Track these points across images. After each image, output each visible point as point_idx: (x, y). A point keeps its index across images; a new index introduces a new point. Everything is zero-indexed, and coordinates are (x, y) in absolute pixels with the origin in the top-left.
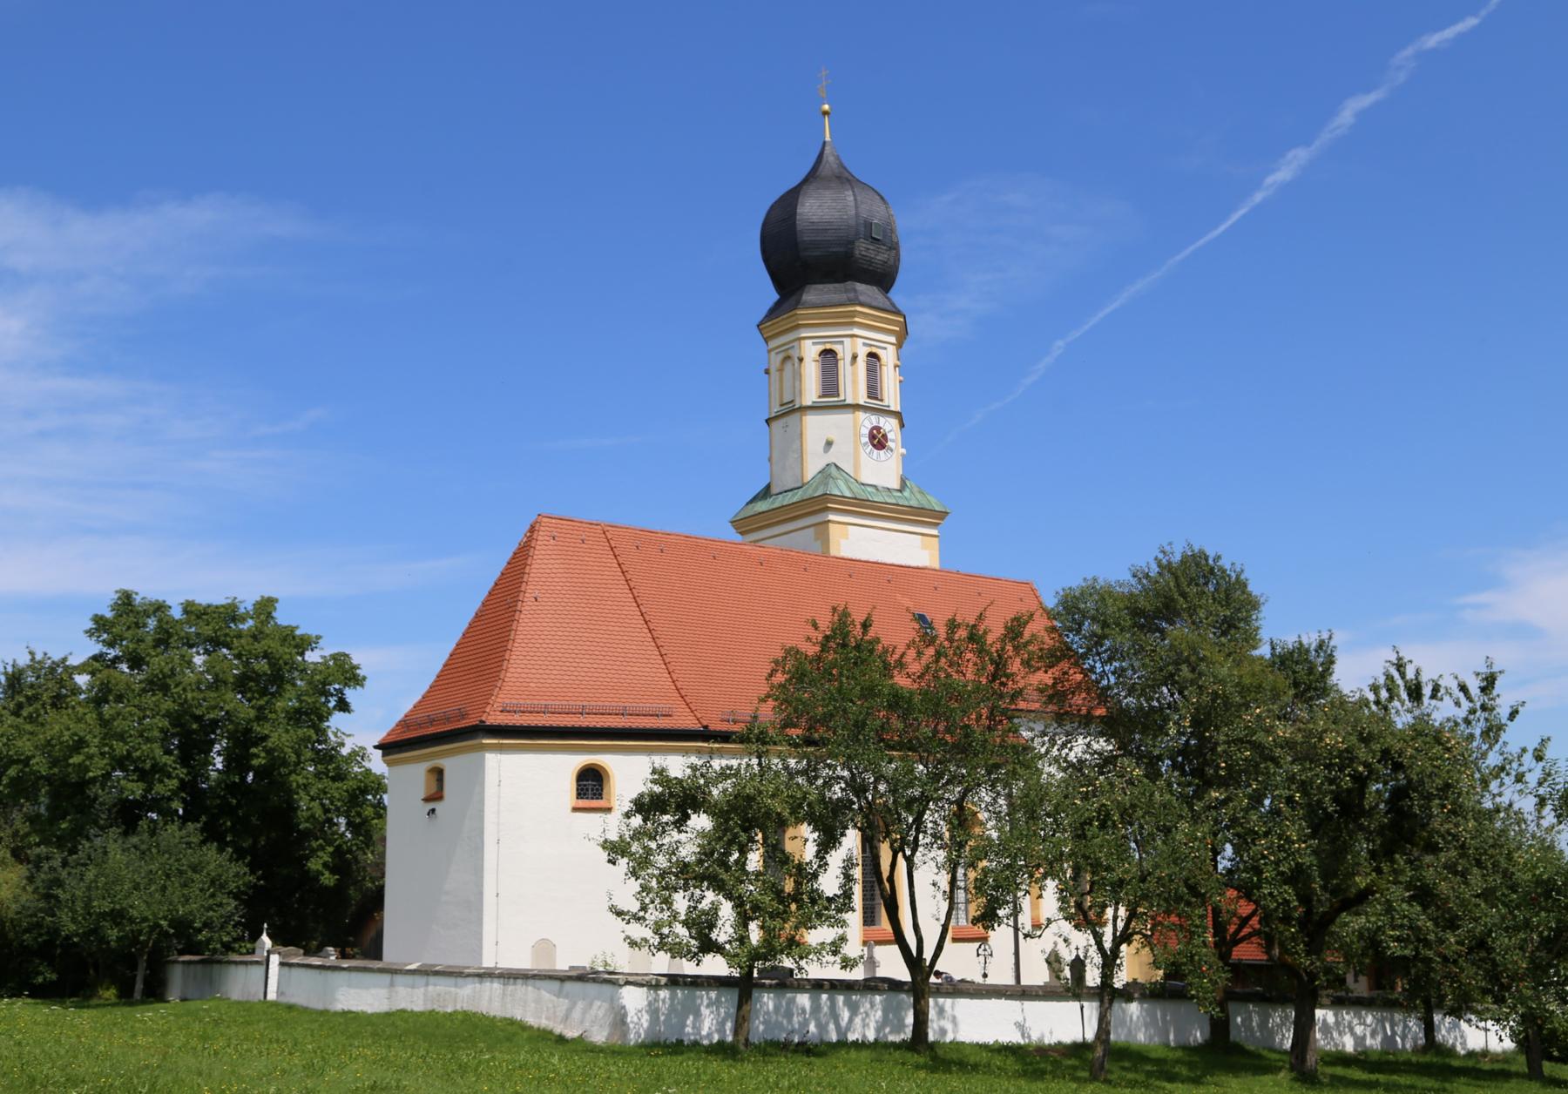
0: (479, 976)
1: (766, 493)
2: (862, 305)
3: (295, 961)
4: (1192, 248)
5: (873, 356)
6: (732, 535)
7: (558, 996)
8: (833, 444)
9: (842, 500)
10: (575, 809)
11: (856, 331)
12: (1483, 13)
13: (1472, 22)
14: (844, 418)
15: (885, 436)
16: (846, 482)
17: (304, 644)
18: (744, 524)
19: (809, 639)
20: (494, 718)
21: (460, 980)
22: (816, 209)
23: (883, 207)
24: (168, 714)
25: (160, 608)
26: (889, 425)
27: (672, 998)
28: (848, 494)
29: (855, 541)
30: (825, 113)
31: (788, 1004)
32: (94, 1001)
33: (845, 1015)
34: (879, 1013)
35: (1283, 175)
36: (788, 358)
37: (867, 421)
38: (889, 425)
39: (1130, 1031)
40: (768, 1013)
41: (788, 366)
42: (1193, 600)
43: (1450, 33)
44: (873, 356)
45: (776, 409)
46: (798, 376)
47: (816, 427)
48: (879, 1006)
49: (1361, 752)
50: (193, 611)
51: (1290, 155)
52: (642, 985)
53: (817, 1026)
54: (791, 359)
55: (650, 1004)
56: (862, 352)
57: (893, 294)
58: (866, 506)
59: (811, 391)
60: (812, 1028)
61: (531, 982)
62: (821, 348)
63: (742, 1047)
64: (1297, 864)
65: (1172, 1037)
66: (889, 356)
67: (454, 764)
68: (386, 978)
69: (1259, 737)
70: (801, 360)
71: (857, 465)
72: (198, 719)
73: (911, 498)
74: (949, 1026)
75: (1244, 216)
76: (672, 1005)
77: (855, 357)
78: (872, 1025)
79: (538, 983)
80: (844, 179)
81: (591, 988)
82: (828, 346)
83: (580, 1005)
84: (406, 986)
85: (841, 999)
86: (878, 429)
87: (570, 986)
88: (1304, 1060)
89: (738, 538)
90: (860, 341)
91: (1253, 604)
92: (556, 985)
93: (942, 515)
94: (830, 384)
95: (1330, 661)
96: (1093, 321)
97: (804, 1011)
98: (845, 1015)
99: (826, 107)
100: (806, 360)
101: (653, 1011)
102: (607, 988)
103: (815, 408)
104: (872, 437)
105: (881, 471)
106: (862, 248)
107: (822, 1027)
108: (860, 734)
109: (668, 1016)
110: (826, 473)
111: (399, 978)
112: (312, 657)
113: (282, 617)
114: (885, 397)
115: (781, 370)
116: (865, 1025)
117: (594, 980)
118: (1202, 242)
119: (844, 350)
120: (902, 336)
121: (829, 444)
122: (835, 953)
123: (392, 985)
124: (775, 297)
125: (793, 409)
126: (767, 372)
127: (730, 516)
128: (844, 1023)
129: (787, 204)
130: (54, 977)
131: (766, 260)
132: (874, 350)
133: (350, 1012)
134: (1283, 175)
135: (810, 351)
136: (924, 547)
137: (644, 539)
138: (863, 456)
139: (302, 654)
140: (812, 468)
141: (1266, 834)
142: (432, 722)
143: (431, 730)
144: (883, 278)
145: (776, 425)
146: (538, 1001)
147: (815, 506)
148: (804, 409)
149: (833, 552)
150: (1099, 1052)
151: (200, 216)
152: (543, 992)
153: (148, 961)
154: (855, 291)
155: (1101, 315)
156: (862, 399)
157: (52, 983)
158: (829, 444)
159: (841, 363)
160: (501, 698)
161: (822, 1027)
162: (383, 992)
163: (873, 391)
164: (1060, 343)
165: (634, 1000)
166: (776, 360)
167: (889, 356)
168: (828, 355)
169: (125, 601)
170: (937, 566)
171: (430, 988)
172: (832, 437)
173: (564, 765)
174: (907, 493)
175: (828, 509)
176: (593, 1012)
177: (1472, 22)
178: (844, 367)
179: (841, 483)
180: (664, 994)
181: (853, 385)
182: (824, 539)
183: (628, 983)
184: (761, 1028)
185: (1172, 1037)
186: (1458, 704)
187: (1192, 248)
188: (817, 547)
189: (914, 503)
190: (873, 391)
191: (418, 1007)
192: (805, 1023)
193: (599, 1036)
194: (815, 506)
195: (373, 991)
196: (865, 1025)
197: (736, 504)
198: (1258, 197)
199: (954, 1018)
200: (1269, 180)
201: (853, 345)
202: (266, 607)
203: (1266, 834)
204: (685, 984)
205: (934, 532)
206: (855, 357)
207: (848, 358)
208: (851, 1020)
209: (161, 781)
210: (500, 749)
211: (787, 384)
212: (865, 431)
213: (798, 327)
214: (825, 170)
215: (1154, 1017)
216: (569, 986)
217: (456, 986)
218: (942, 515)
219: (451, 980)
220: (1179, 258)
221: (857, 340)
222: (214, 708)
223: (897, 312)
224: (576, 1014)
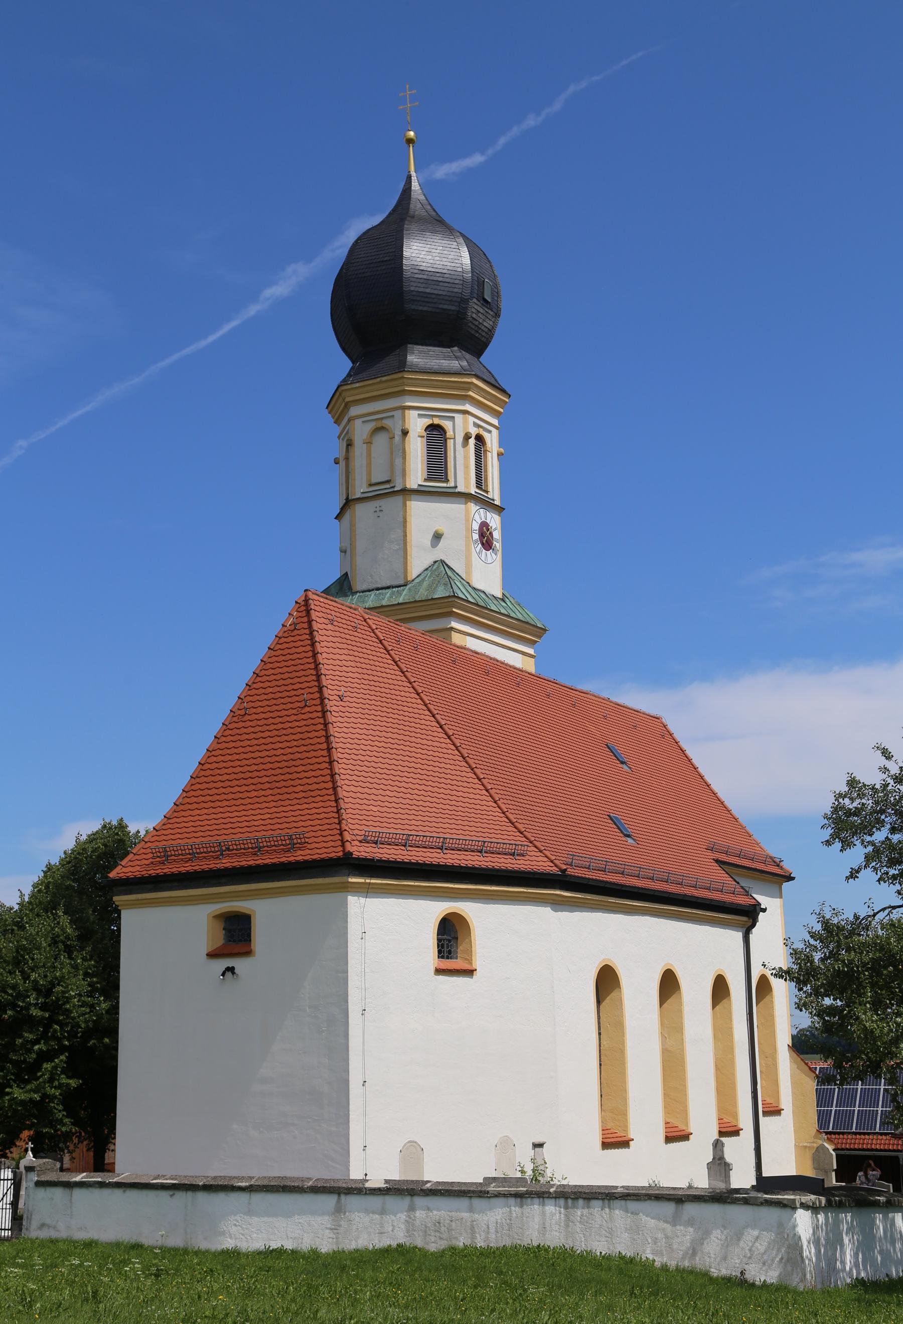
0: (518, 1196)
2: (477, 377)
3: (78, 1178)
7: (674, 1224)
10: (439, 971)
12: (490, 151)
13: (478, 159)
21: (477, 1202)
30: (410, 141)
35: (278, 290)
37: (478, 515)
43: (456, 167)
44: (479, 438)
47: (423, 516)
51: (290, 269)
59: (416, 473)
61: (617, 1203)
62: (428, 421)
67: (273, 913)
70: (405, 433)
71: (468, 565)
79: (632, 1205)
82: (436, 421)
84: (367, 1211)
90: (471, 420)
92: (669, 1208)
94: (437, 465)
96: (61, 423)
99: (412, 134)
100: (411, 434)
103: (421, 492)
114: (490, 489)
115: (369, 443)
118: (187, 351)
119: (459, 427)
121: (438, 537)
123: (339, 1210)
125: (392, 491)
133: (279, 1253)
134: (278, 290)
135: (417, 424)
138: (474, 556)
142: (258, 850)
143: (226, 863)
148: (406, 492)
152: (644, 1218)
158: (438, 537)
159: (450, 443)
164: (23, 443)
168: (436, 433)
171: (419, 1214)
172: (441, 527)
173: (422, 913)
175: (451, 614)
177: (478, 159)
190: (480, 481)
193: (764, 1273)
198: (253, 310)
200: (268, 292)
205: (531, 651)
207: (460, 439)
210: (367, 891)
212: (476, 527)
213: (403, 393)
216: (691, 1209)
217: (471, 1210)
219: (464, 1202)
220: (162, 364)
221: (448, 419)
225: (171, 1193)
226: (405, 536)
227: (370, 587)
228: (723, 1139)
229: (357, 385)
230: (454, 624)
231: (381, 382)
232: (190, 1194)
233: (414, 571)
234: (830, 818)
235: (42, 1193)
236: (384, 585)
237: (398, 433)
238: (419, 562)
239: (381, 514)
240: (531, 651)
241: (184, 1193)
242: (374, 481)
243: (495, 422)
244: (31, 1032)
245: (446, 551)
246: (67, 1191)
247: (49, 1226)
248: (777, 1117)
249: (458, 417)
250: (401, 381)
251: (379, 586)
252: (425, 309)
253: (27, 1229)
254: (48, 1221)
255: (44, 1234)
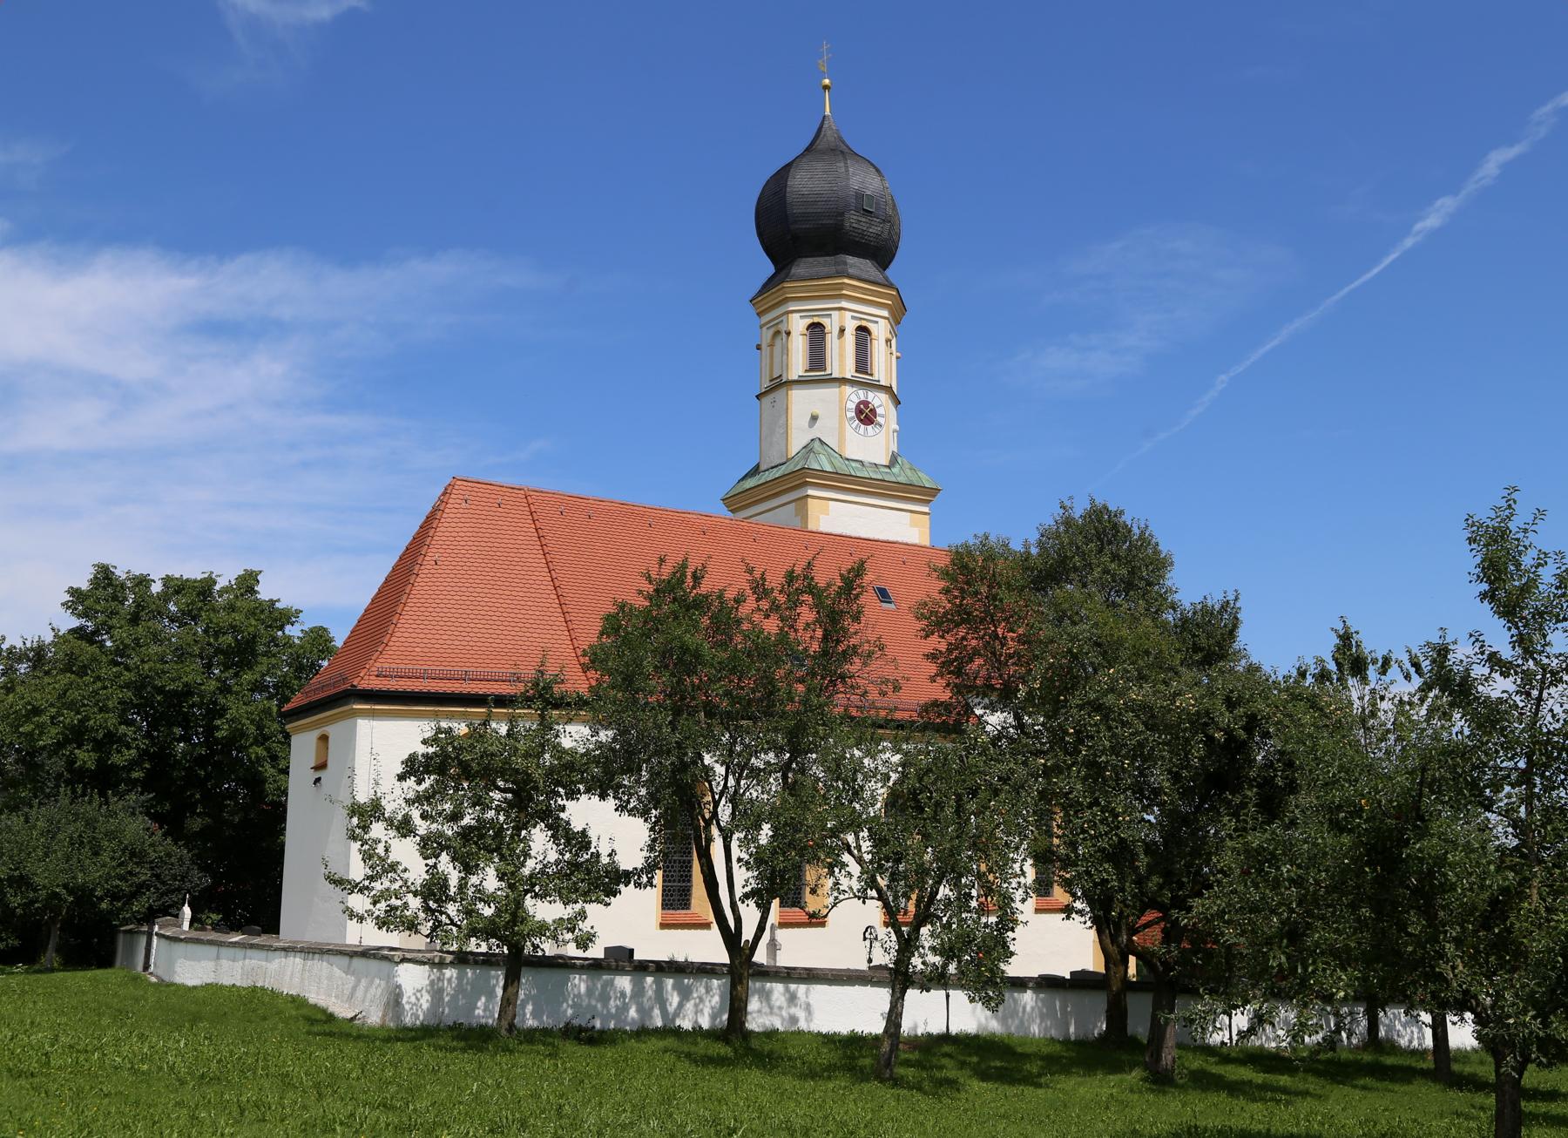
1: (755, 471)
4: (1346, 290)
5: (863, 330)
6: (723, 511)
8: (817, 418)
9: (821, 474)
11: (844, 304)
14: (830, 392)
15: (873, 411)
16: (829, 457)
17: (287, 617)
18: (736, 501)
19: (640, 592)
20: (369, 682)
22: (803, 183)
23: (877, 179)
24: (127, 686)
25: (143, 582)
26: (879, 400)
27: (460, 978)
28: (828, 468)
29: (838, 516)
30: (826, 87)
31: (604, 987)
32: (37, 967)
33: (674, 1000)
34: (716, 999)
35: (1432, 221)
36: (778, 333)
37: (853, 396)
38: (879, 400)
39: (1022, 1022)
40: (579, 995)
41: (778, 342)
42: (1102, 554)
45: (766, 384)
46: (786, 351)
48: (716, 991)
49: (1225, 718)
50: (176, 587)
51: (1439, 203)
52: (423, 963)
53: (638, 1011)
54: (781, 334)
55: (432, 983)
56: (851, 326)
57: (888, 272)
58: (853, 482)
59: (798, 365)
60: (633, 1013)
62: (809, 321)
63: (503, 1032)
64: (1122, 840)
65: (1072, 1029)
66: (880, 330)
68: (213, 950)
69: (1110, 699)
70: (788, 334)
72: (160, 690)
73: (900, 474)
74: (801, 1014)
75: (1394, 261)
76: (460, 984)
77: (842, 331)
78: (707, 1011)
80: (841, 151)
81: (373, 965)
82: (816, 320)
83: (364, 982)
85: (669, 982)
86: (866, 403)
87: (358, 963)
88: (1159, 1058)
89: (731, 515)
90: (849, 314)
91: (1160, 565)
92: (345, 960)
93: (934, 492)
94: (817, 358)
95: (1235, 623)
97: (623, 994)
98: (674, 1000)
99: (827, 81)
100: (793, 334)
101: (436, 992)
102: (385, 965)
103: (801, 382)
104: (859, 412)
105: (871, 447)
106: (853, 220)
107: (645, 1012)
108: (703, 694)
109: (454, 998)
110: (808, 449)
111: (224, 951)
112: (293, 631)
113: (265, 592)
115: (771, 345)
116: (698, 1011)
117: (375, 957)
119: (831, 324)
120: (898, 313)
121: (814, 418)
122: (572, 930)
123: (218, 958)
124: (768, 268)
125: (780, 384)
126: (759, 347)
127: (722, 495)
128: (671, 1009)
129: (780, 179)
130: (16, 943)
131: (760, 235)
132: (864, 323)
134: (1432, 221)
135: (798, 325)
136: (913, 524)
137: (572, 504)
138: (849, 431)
139: (282, 628)
140: (796, 444)
141: (1090, 806)
144: (881, 253)
145: (767, 400)
146: (330, 978)
147: (795, 481)
149: (811, 527)
150: (886, 1047)
151: (442, 270)
153: (61, 929)
154: (845, 263)
155: (1262, 351)
156: (850, 371)
157: (14, 948)
158: (814, 418)
159: (828, 337)
160: (383, 662)
161: (645, 1012)
162: (210, 965)
163: (863, 364)
164: (1223, 377)
165: (412, 978)
166: (767, 334)
167: (880, 330)
168: (816, 330)
169: (104, 576)
170: (927, 543)
172: (816, 411)
174: (896, 470)
176: (372, 991)
178: (832, 341)
179: (823, 458)
180: (450, 973)
181: (841, 358)
182: (803, 514)
183: (404, 960)
184: (570, 1012)
185: (1072, 1029)
186: (1408, 677)
187: (1346, 290)
188: (797, 523)
189: (902, 479)
190: (863, 364)
191: (239, 981)
192: (625, 1008)
193: (374, 1018)
194: (795, 481)
195: (204, 963)
196: (698, 1011)
197: (729, 478)
198: (1409, 242)
199: (808, 1005)
200: (1418, 226)
201: (842, 319)
202: (248, 582)
203: (1090, 806)
204: (476, 963)
205: (926, 509)
206: (842, 331)
207: (836, 332)
208: (681, 1006)
209: (119, 752)
210: (373, 715)
211: (777, 360)
213: (786, 300)
214: (821, 145)
215: (1051, 1008)
218: (934, 492)
219: (263, 954)
221: (849, 312)
222: (173, 680)
223: (890, 286)
224: (359, 993)
230: (811, 492)
233: (793, 450)
238: (797, 441)
240: (926, 509)
243: (885, 313)
245: (824, 430)
248: (820, 929)
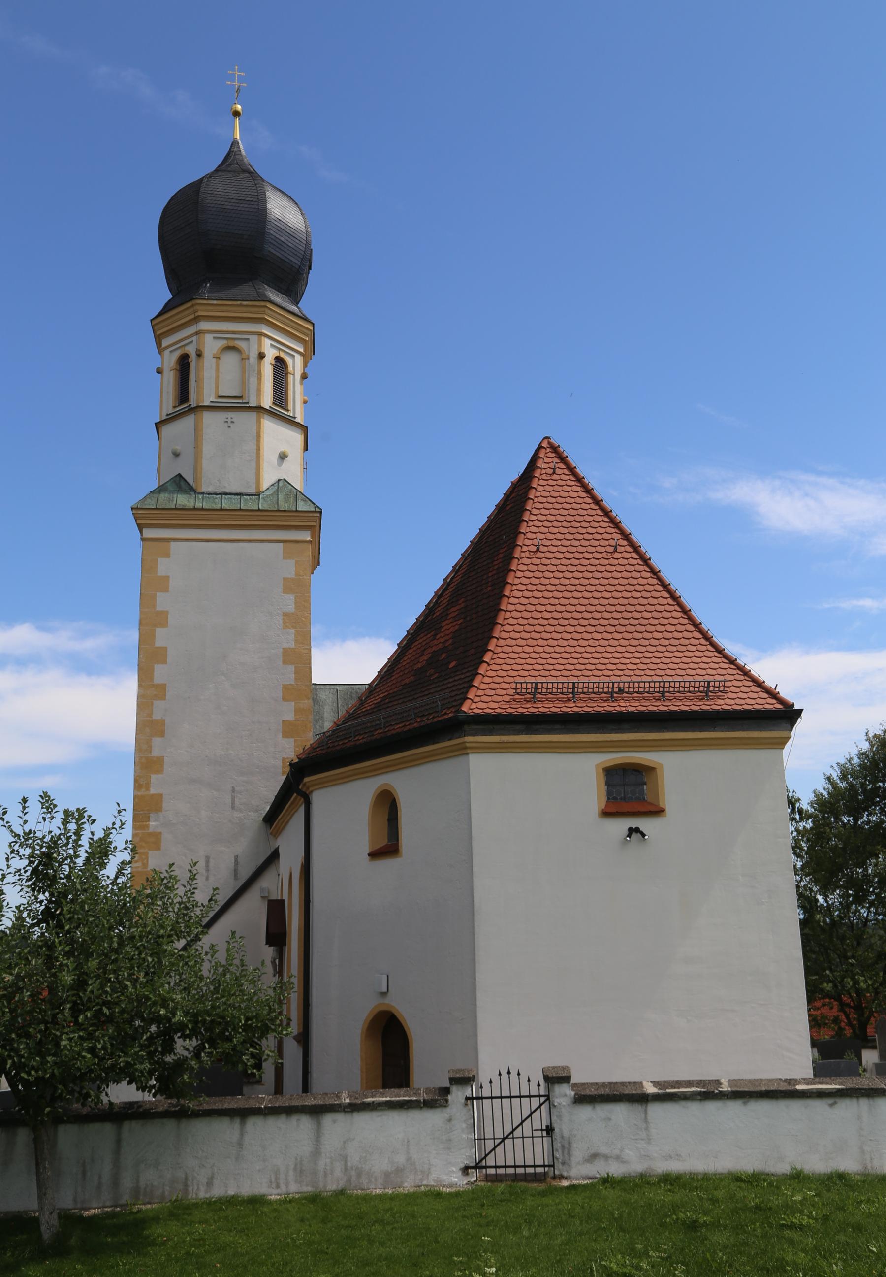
30: (236, 114)
62: (223, 343)
82: (282, 355)
90: (267, 342)
99: (239, 107)
213: (197, 319)
225: (830, 1101)
226: (258, 449)
227: (218, 491)
228: (448, 1085)
229: (215, 302)
231: (241, 305)
232: (864, 1102)
234: (851, 764)
235: (586, 1112)
236: (234, 492)
237: (254, 355)
239: (231, 425)
241: (855, 1101)
242: (221, 394)
244: (817, 900)
246: (638, 1108)
247: (606, 1157)
249: (254, 338)
250: (263, 309)
251: (228, 491)
252: (278, 254)
253: (563, 1163)
254: (603, 1150)
255: (599, 1169)
